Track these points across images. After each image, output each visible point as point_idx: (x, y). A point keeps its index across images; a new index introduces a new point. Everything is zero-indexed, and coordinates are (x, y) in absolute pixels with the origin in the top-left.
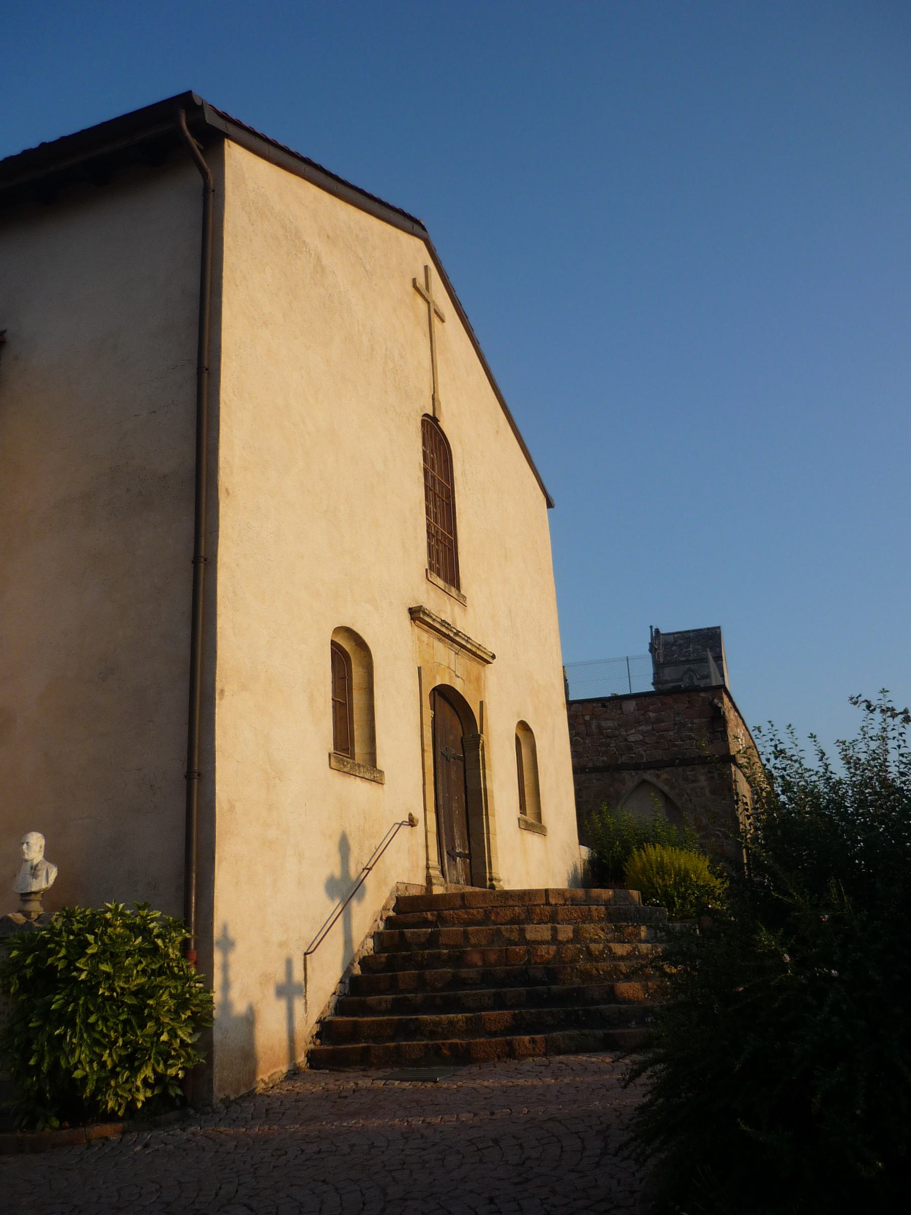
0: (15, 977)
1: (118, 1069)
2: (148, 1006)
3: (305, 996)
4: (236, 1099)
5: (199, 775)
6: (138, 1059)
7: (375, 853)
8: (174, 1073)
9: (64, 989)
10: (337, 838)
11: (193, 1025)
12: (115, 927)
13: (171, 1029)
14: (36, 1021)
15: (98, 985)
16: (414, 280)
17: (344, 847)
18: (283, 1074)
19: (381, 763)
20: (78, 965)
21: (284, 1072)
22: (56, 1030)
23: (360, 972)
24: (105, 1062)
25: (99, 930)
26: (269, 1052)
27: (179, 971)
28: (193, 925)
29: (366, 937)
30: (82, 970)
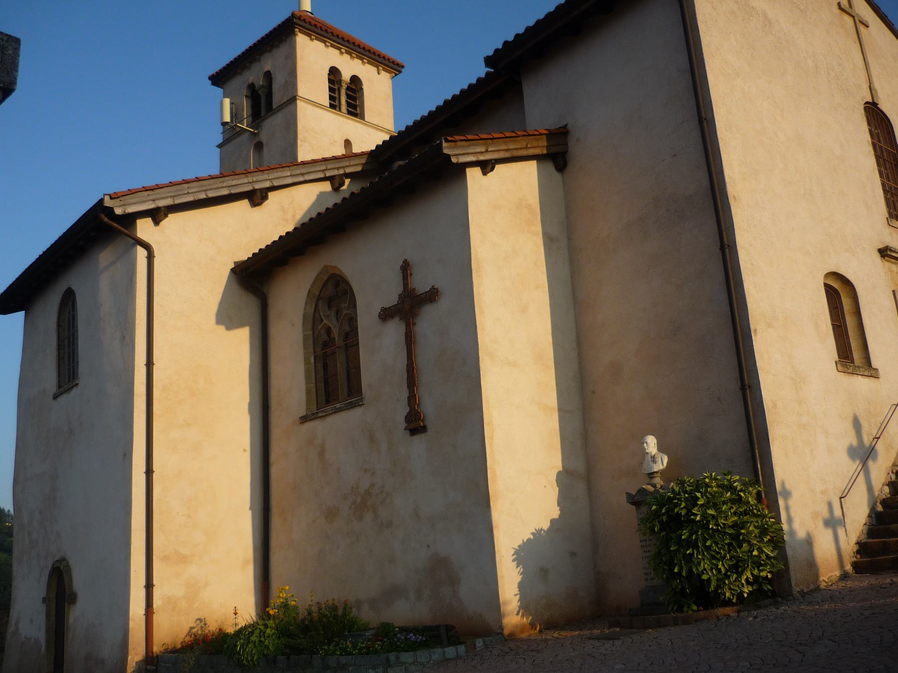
0: (657, 521)
1: (729, 573)
2: (741, 534)
3: (845, 526)
4: (808, 592)
5: (749, 387)
6: (741, 567)
7: (880, 427)
8: (765, 575)
9: (687, 527)
10: (851, 419)
11: (772, 545)
12: (712, 487)
13: (758, 548)
14: (674, 546)
15: (708, 522)
16: (839, 4)
17: (857, 424)
18: (837, 577)
19: (874, 363)
20: (694, 511)
21: (838, 575)
22: (687, 551)
23: (882, 510)
24: (720, 569)
25: (702, 490)
26: (825, 562)
27: (757, 512)
28: (761, 483)
29: (883, 485)
30: (697, 515)
